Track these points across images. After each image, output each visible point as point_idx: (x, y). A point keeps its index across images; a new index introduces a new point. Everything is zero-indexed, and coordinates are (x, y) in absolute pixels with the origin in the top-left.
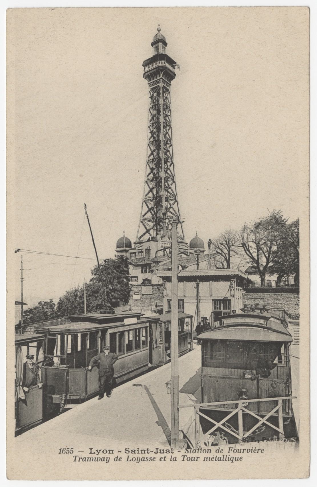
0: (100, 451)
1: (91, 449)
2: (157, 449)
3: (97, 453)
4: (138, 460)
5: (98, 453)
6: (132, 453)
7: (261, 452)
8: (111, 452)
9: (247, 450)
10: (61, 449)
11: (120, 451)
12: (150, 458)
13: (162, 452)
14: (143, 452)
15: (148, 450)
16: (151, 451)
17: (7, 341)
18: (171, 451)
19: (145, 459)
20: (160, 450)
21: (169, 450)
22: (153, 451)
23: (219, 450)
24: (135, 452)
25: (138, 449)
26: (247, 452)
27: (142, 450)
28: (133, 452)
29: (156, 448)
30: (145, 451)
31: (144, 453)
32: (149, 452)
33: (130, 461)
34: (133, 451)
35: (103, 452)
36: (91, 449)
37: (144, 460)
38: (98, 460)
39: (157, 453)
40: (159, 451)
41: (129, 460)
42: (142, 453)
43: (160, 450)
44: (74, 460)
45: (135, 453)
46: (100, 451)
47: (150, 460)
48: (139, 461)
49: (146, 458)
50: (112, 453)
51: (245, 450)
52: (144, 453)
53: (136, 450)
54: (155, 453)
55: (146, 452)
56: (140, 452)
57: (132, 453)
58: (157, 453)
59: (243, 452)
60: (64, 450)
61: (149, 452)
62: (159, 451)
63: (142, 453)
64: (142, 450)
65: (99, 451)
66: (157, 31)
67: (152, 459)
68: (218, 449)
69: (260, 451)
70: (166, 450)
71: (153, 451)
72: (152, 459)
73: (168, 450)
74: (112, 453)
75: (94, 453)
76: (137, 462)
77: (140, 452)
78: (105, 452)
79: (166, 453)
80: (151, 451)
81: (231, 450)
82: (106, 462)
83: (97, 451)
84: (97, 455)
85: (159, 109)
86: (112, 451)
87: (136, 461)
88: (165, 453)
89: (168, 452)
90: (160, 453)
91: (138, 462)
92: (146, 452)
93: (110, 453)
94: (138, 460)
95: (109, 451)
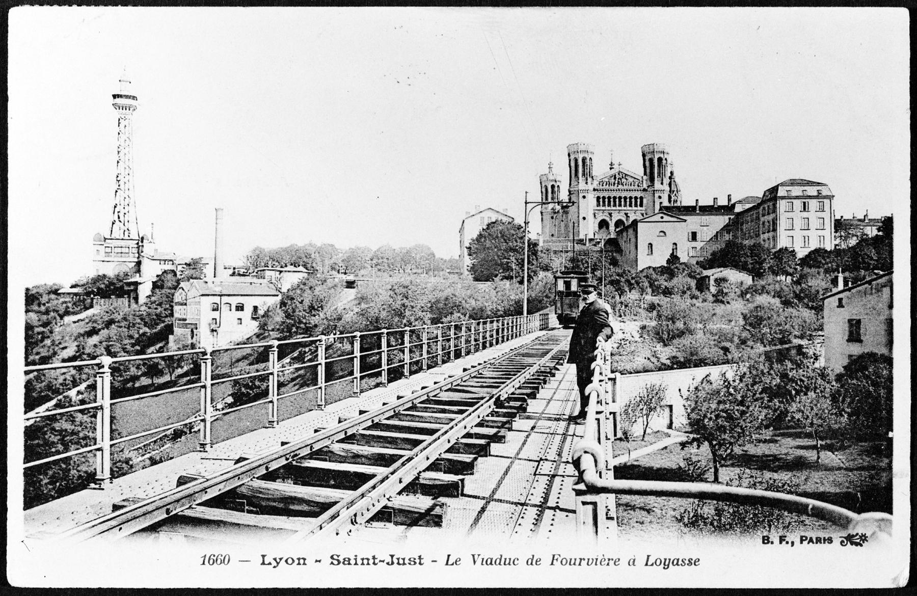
0: (281, 559)
1: (263, 556)
2: (392, 556)
3: (274, 564)
4: (667, 563)
5: (278, 563)
6: (344, 563)
7: (615, 564)
8: (302, 562)
9: (586, 560)
10: (205, 556)
11: (318, 560)
12: (689, 561)
13: (401, 561)
14: (365, 562)
15: (374, 558)
16: (380, 561)
17: (224, 435)
18: (417, 561)
19: (680, 562)
20: (398, 559)
21: (415, 559)
22: (383, 561)
23: (532, 560)
24: (351, 562)
25: (356, 556)
26: (588, 564)
27: (363, 559)
28: (346, 562)
29: (390, 555)
30: (368, 559)
31: (368, 564)
32: (376, 561)
33: (652, 565)
34: (347, 559)
35: (286, 561)
36: (263, 556)
37: (677, 564)
38: (590, 563)
39: (393, 563)
40: (395, 561)
41: (649, 563)
42: (363, 564)
43: (398, 559)
44: (650, 557)
45: (349, 564)
46: (281, 559)
47: (683, 564)
48: (668, 565)
49: (682, 561)
50: (304, 564)
51: (584, 559)
52: (368, 564)
53: (352, 558)
54: (388, 564)
55: (371, 561)
56: (359, 562)
57: (344, 563)
58: (393, 563)
59: (580, 565)
60: (212, 557)
61: (376, 561)
62: (395, 561)
63: (363, 564)
64: (363, 559)
65: (278, 560)
66: (254, 322)
67: (693, 562)
68: (532, 557)
69: (613, 561)
70: (410, 559)
71: (383, 561)
72: (693, 562)
73: (412, 559)
74: (304, 564)
75: (270, 564)
76: (664, 568)
77: (359, 562)
78: (290, 561)
79: (410, 564)
80: (380, 561)
81: (557, 560)
82: (664, 568)
83: (275, 559)
84: (275, 567)
85: (292, 337)
86: (304, 559)
87: (662, 565)
88: (408, 564)
89: (412, 563)
90: (398, 563)
91: (666, 567)
92: (371, 561)
93: (299, 564)
94: (667, 563)
95: (299, 559)
